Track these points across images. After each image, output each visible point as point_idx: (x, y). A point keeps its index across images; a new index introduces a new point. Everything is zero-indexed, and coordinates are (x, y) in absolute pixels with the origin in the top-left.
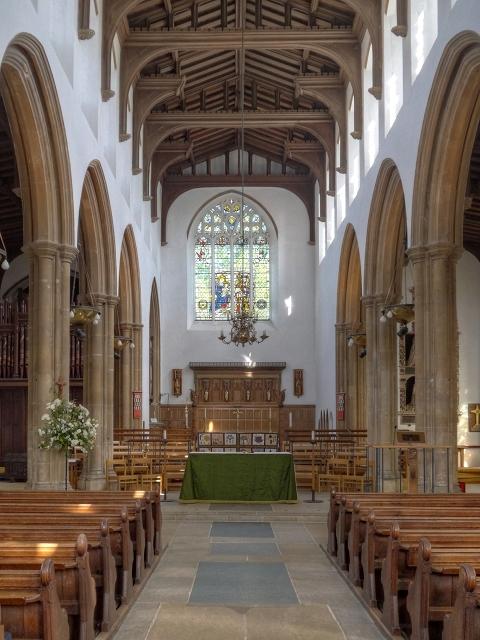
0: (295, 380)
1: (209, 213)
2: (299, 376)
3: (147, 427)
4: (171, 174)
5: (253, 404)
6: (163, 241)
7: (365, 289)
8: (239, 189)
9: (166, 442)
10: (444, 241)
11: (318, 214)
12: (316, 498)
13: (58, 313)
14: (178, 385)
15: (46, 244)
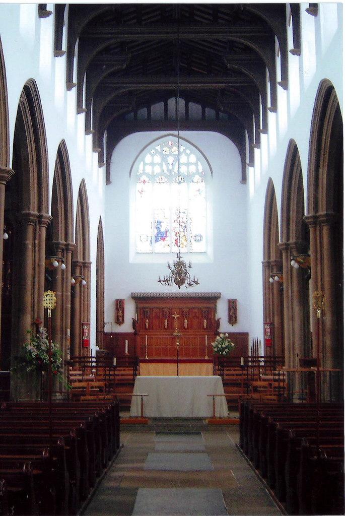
0: (230, 309)
1: (150, 153)
2: (233, 305)
3: (94, 354)
4: (113, 121)
6: (108, 180)
7: (282, 237)
8: (176, 133)
9: (115, 367)
10: (300, 241)
11: (248, 161)
12: (212, 397)
13: (37, 265)
14: (120, 314)
15: (29, 214)
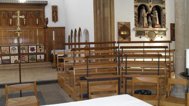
0: (53, 12)
2: (55, 9)
5: (28, 27)
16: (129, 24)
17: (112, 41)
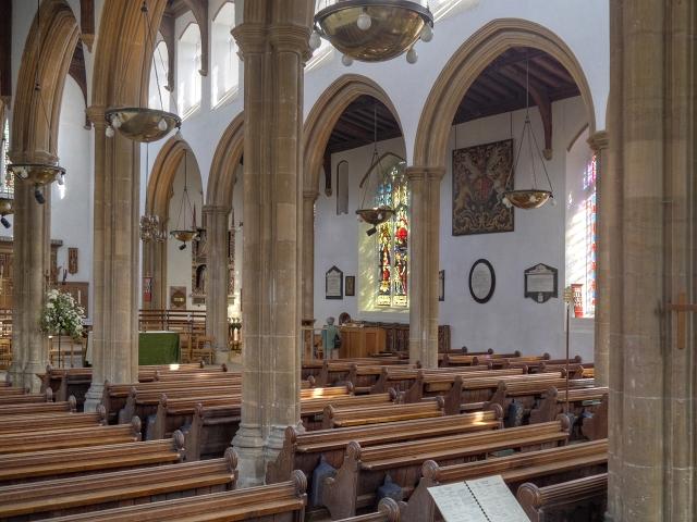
0: (70, 258)
16: (185, 288)
17: (281, 446)
